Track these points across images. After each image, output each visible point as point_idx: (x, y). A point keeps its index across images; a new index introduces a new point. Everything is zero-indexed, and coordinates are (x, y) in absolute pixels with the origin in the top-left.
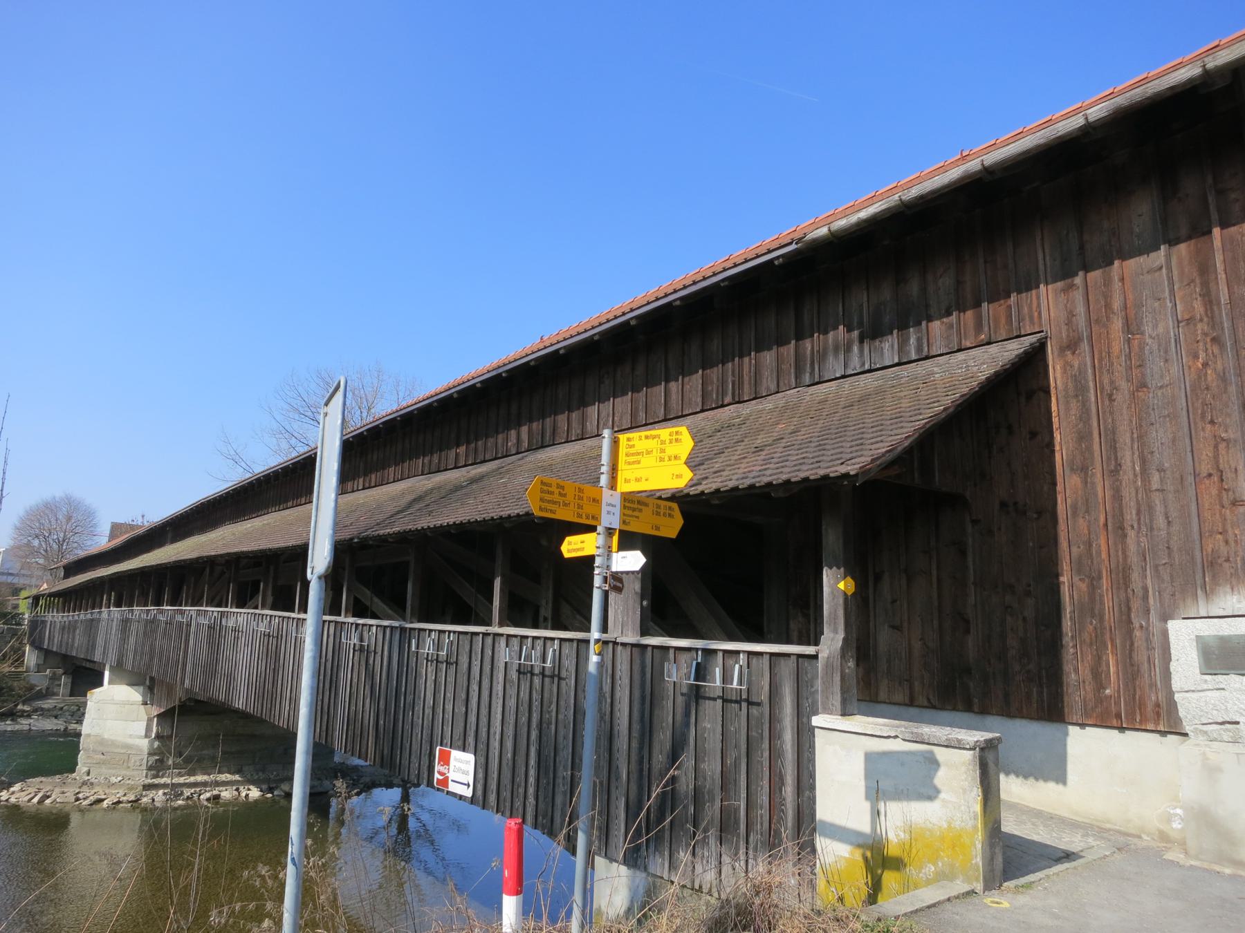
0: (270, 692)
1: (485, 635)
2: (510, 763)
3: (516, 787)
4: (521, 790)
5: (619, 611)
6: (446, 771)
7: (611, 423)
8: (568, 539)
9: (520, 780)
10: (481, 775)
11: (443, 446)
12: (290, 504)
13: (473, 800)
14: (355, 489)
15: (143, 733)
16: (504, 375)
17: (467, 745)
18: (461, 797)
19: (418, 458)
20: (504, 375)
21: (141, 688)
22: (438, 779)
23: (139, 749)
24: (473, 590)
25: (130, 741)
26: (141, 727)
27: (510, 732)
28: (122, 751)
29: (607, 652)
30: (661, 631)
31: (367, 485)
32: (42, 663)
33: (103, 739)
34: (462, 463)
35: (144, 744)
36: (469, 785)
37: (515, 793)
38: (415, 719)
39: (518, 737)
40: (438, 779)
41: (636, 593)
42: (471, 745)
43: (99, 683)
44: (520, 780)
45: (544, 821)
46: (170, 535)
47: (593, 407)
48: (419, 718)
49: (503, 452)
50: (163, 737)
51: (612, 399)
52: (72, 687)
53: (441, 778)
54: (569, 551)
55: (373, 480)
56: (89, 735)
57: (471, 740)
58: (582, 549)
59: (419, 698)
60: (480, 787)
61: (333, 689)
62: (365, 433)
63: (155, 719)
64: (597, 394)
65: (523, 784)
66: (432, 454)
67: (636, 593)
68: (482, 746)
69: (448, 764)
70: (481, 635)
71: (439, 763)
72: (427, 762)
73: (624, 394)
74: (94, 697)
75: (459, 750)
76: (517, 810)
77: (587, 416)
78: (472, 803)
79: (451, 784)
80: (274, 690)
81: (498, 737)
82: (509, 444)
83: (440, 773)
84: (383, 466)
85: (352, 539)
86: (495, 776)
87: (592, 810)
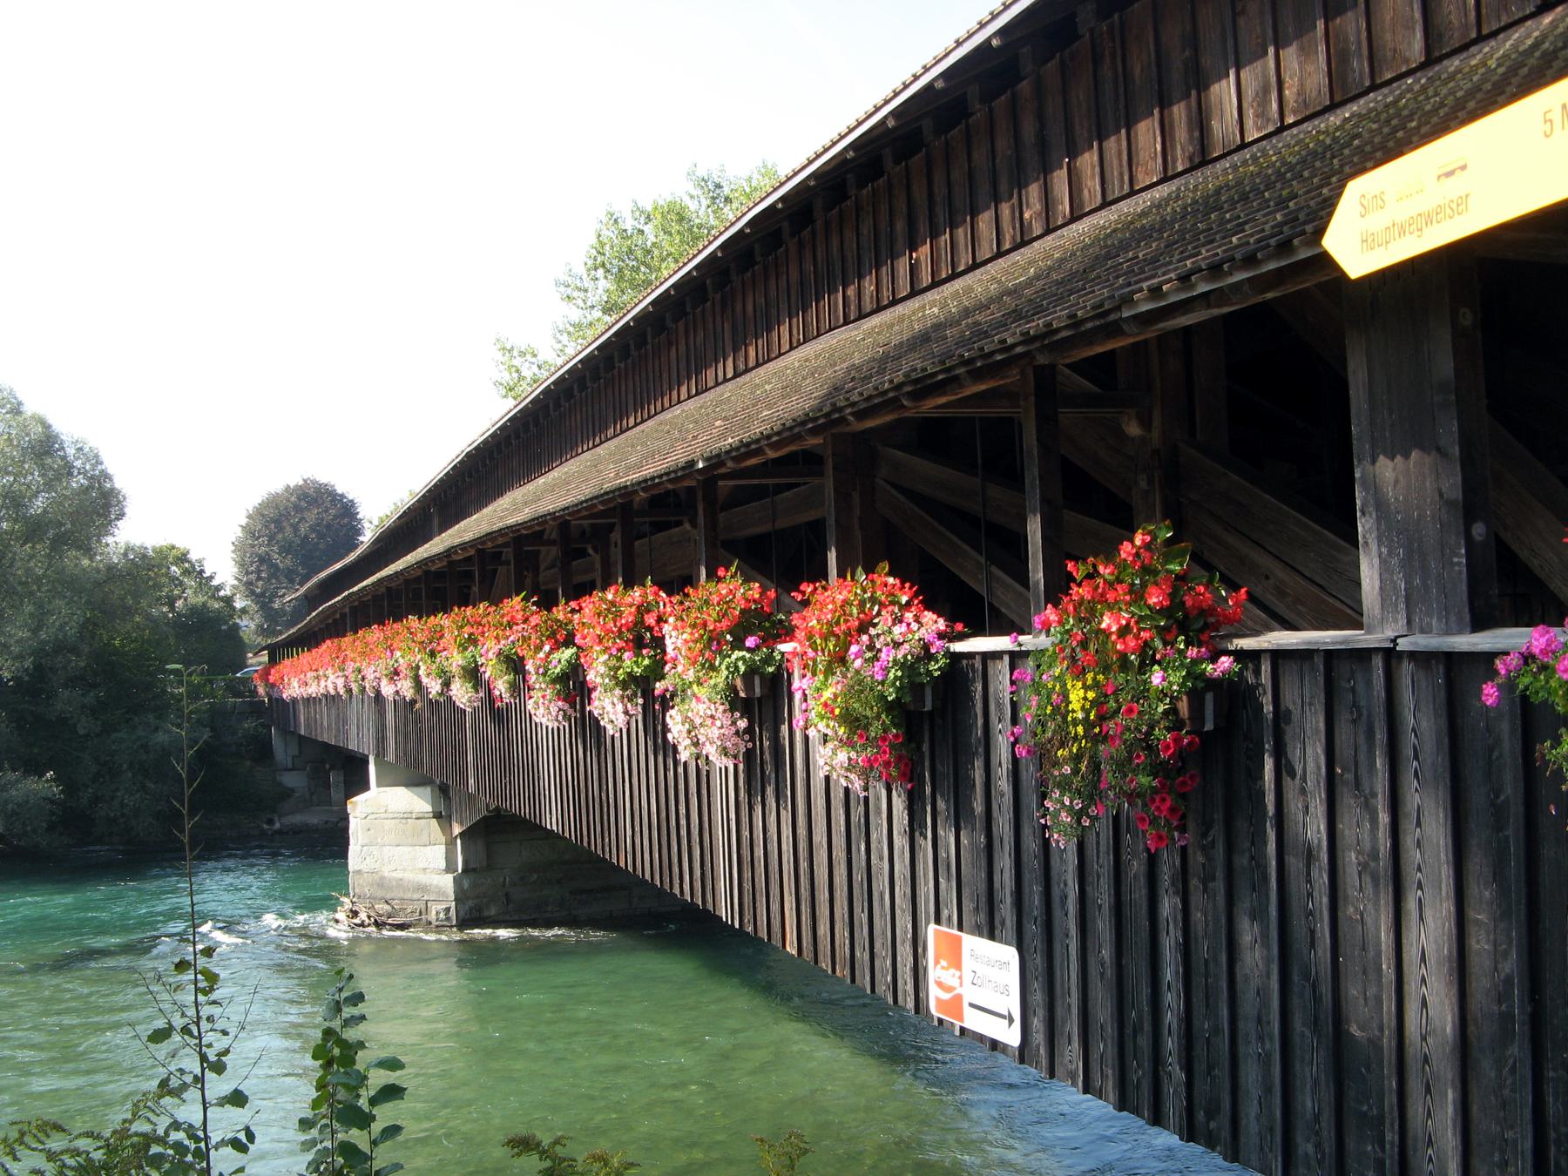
0: (597, 800)
1: (1016, 657)
2: (1110, 972)
3: (1129, 1031)
4: (1144, 1041)
5: (1394, 561)
6: (954, 982)
7: (1275, 106)
8: (1356, 189)
9: (1140, 1018)
10: (1038, 997)
11: (882, 253)
12: (611, 432)
13: (1024, 1053)
14: (720, 379)
15: (443, 865)
16: (995, 42)
17: (997, 923)
18: (995, 1045)
19: (832, 291)
20: (995, 42)
21: (428, 790)
22: (938, 1000)
23: (440, 892)
24: (982, 560)
25: (424, 879)
26: (436, 855)
27: (1103, 896)
28: (416, 896)
29: (1369, 683)
30: (1275, 625)
31: (742, 367)
32: (297, 753)
33: (382, 878)
34: (926, 279)
35: (447, 882)
36: (1011, 1021)
37: (1129, 1046)
38: (874, 861)
39: (1126, 911)
40: (938, 1000)
41: (1450, 504)
42: (1008, 923)
43: (364, 786)
44: (1140, 1018)
45: (1212, 1125)
46: (436, 521)
47: (1224, 83)
48: (881, 859)
49: (1014, 237)
50: (474, 870)
51: (1271, 50)
52: (345, 790)
53: (946, 996)
54: (1368, 242)
55: (752, 353)
56: (359, 872)
57: (1006, 910)
58: (1460, 204)
59: (879, 812)
60: (1037, 1023)
61: (704, 792)
62: (719, 254)
63: (459, 841)
64: (1230, 43)
65: (1147, 1026)
66: (861, 277)
67: (1450, 504)
68: (1033, 929)
69: (958, 966)
70: (1006, 658)
71: (937, 962)
72: (911, 959)
73: (1303, 29)
74: (359, 807)
75: (981, 935)
76: (1138, 1087)
77: (1209, 107)
78: (1022, 1060)
79: (968, 1011)
80: (604, 798)
81: (1072, 906)
82: (1027, 215)
83: (940, 984)
84: (767, 323)
85: (692, 463)
86: (1074, 1000)
87: (846, 420)
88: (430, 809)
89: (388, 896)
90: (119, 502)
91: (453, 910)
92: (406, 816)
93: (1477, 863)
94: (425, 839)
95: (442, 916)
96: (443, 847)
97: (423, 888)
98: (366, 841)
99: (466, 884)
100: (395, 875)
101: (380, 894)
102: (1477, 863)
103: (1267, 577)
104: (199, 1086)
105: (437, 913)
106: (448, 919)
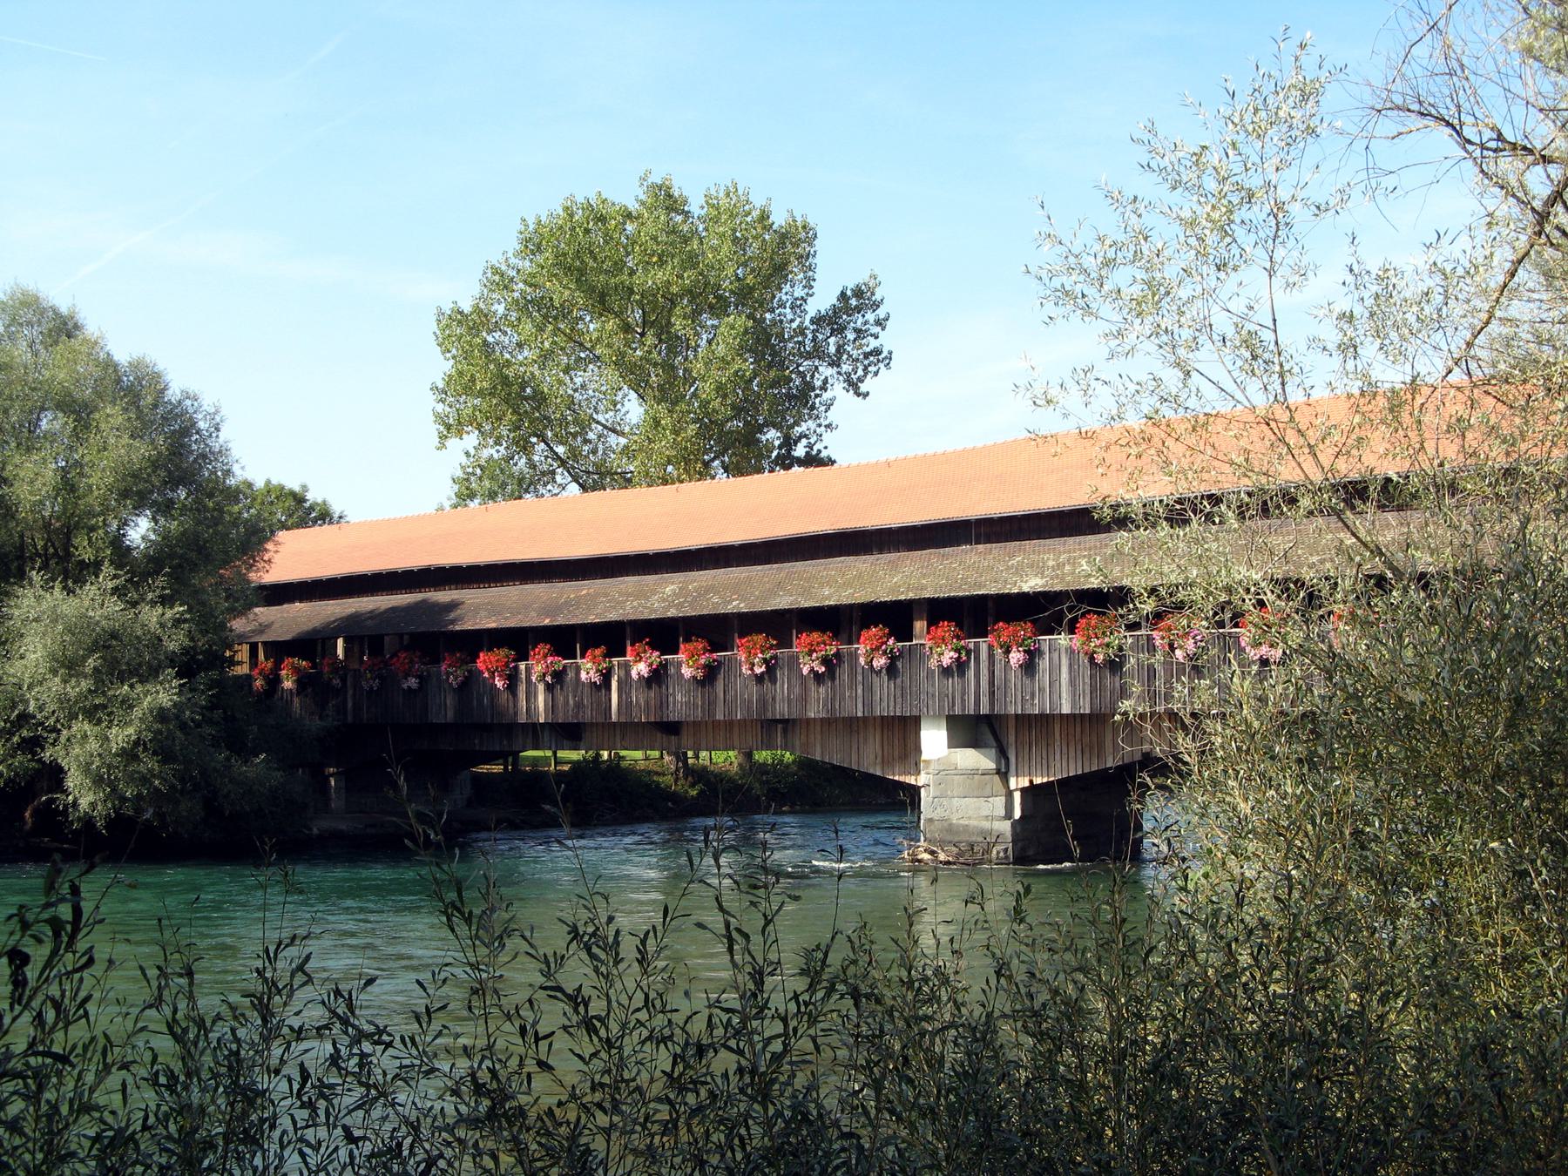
15: (1002, 812)
25: (986, 825)
33: (951, 825)
56: (931, 820)
88: (993, 766)
89: (956, 839)
90: (139, 380)
91: (1010, 849)
92: (974, 773)
93: (885, 743)
94: (988, 791)
95: (1002, 854)
96: (1003, 798)
97: (985, 833)
98: (938, 794)
99: (1018, 830)
100: (961, 822)
101: (949, 838)
102: (885, 743)
103: (1293, 501)
104: (335, 1155)
105: (998, 853)
106: (1007, 857)
